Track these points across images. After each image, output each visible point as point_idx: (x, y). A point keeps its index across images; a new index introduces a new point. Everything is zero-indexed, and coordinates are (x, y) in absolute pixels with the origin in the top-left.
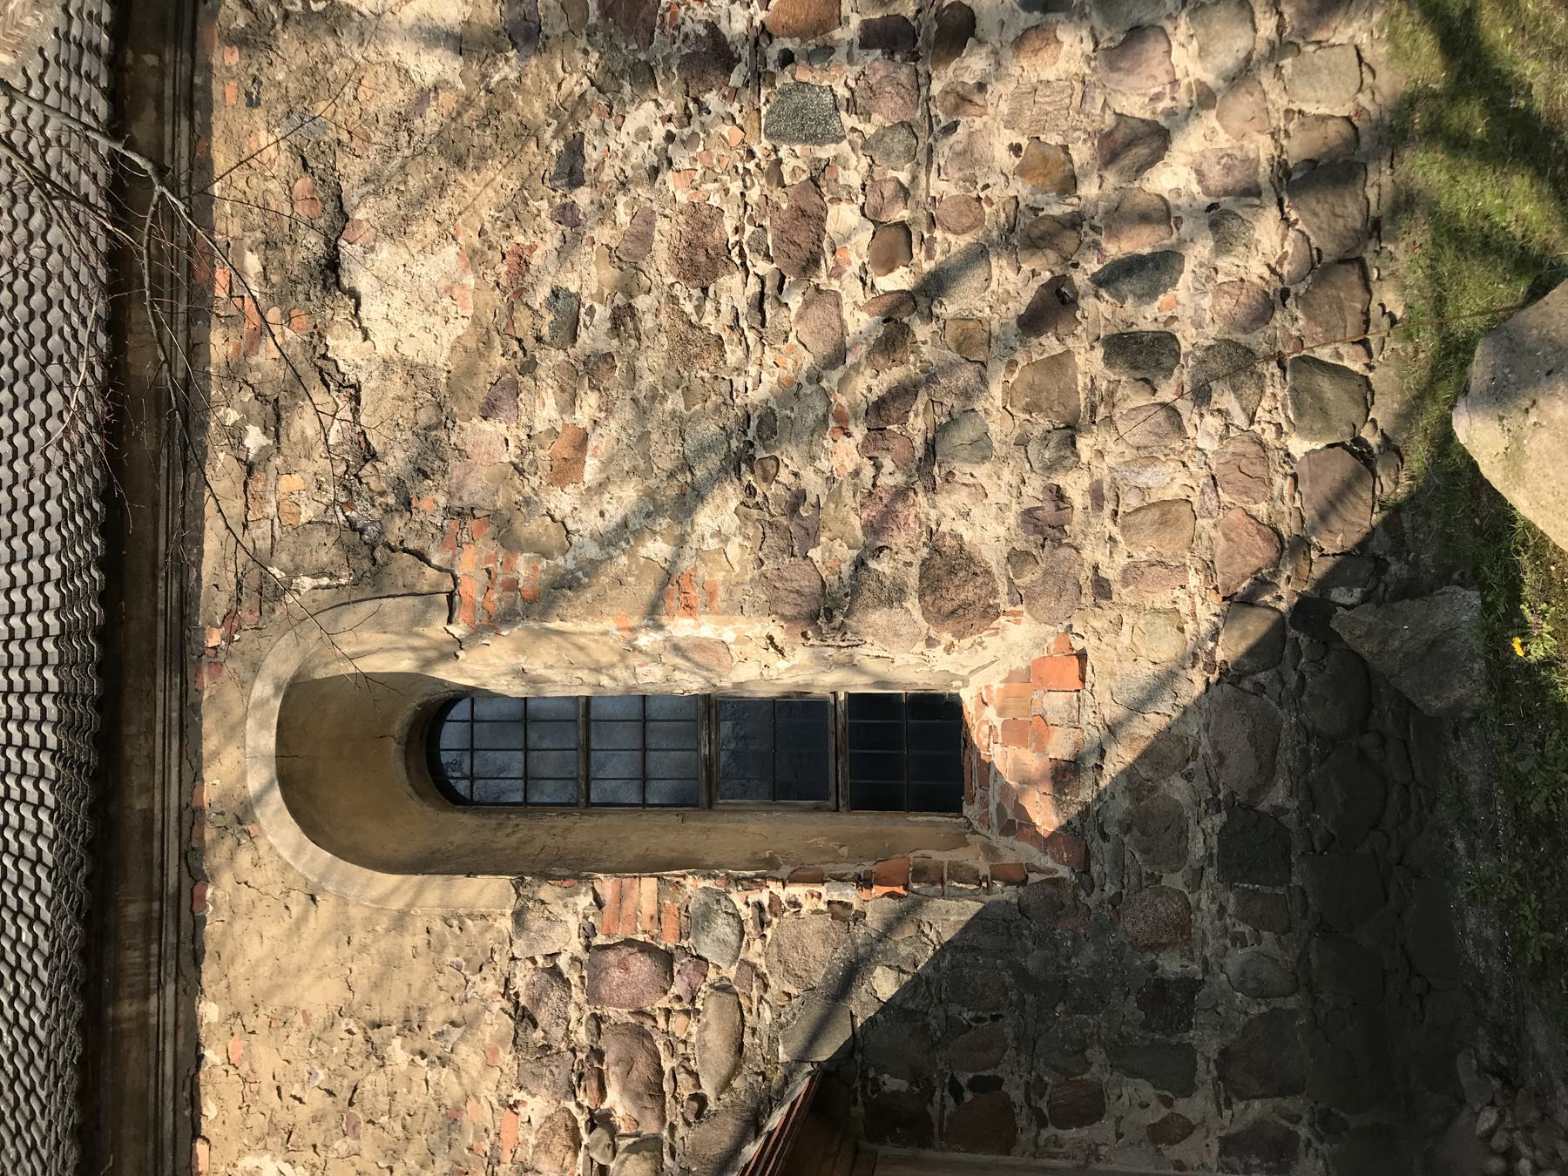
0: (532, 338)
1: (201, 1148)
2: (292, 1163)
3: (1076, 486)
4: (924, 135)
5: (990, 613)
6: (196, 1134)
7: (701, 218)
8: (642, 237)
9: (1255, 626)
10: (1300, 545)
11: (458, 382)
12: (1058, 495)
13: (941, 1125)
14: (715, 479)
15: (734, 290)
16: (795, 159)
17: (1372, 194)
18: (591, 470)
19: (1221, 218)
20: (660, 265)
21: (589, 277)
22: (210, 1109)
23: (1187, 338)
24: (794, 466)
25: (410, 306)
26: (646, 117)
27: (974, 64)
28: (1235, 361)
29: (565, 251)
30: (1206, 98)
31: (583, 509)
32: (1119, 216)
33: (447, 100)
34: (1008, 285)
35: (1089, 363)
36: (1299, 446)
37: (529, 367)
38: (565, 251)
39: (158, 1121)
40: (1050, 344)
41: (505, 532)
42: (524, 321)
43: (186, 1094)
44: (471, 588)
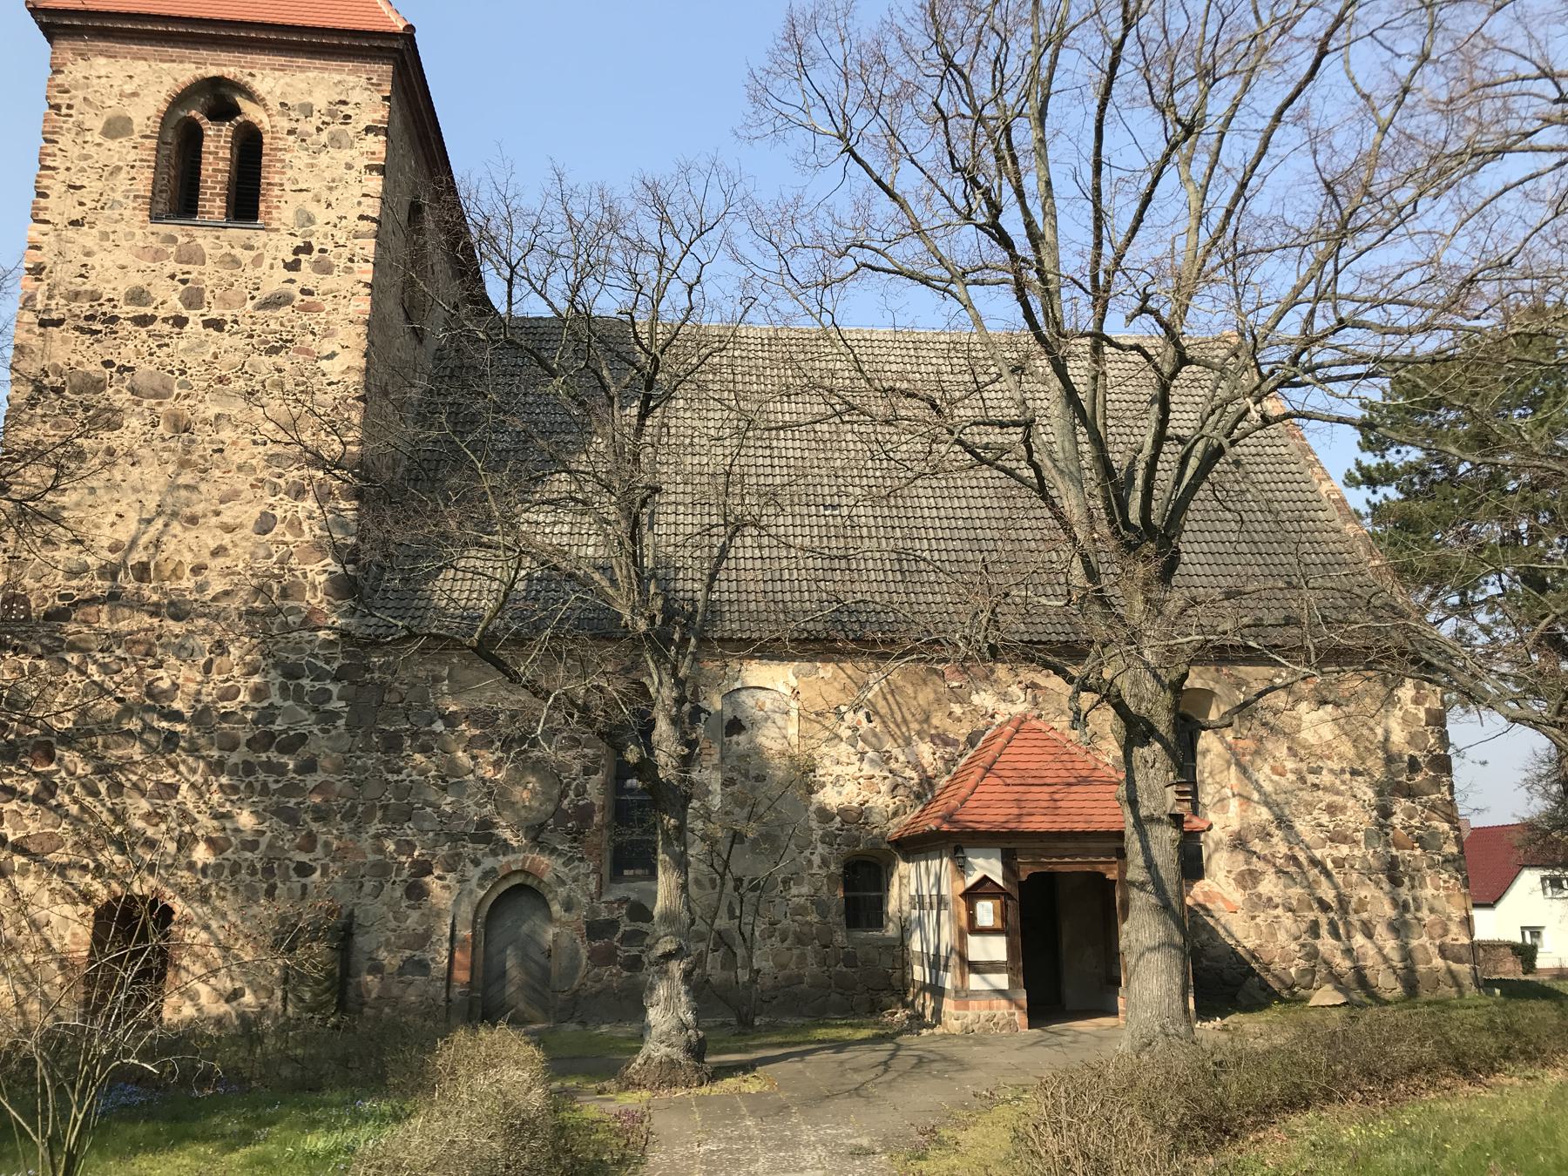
0: (1309, 760)
3: (1280, 911)
4: (1368, 872)
5: (1244, 888)
7: (1343, 809)
8: (1338, 793)
9: (1247, 957)
10: (1268, 970)
11: (1293, 740)
12: (1276, 907)
14: (1274, 814)
15: (1325, 819)
16: (1360, 836)
17: (1131, 59)
18: (1276, 778)
19: (1348, 952)
20: (1329, 798)
21: (1326, 778)
23: (1318, 943)
24: (1278, 836)
25: (1316, 725)
26: (1369, 795)
27: (1386, 886)
28: (1313, 954)
29: (1331, 771)
30: (1380, 950)
31: (1263, 773)
32: (1347, 924)
33: (1371, 737)
34: (1329, 895)
35: (1311, 916)
36: (1293, 970)
37: (1302, 760)
38: (1331, 771)
40: (1316, 906)
41: (1257, 753)
42: (1313, 759)
44: (1241, 743)
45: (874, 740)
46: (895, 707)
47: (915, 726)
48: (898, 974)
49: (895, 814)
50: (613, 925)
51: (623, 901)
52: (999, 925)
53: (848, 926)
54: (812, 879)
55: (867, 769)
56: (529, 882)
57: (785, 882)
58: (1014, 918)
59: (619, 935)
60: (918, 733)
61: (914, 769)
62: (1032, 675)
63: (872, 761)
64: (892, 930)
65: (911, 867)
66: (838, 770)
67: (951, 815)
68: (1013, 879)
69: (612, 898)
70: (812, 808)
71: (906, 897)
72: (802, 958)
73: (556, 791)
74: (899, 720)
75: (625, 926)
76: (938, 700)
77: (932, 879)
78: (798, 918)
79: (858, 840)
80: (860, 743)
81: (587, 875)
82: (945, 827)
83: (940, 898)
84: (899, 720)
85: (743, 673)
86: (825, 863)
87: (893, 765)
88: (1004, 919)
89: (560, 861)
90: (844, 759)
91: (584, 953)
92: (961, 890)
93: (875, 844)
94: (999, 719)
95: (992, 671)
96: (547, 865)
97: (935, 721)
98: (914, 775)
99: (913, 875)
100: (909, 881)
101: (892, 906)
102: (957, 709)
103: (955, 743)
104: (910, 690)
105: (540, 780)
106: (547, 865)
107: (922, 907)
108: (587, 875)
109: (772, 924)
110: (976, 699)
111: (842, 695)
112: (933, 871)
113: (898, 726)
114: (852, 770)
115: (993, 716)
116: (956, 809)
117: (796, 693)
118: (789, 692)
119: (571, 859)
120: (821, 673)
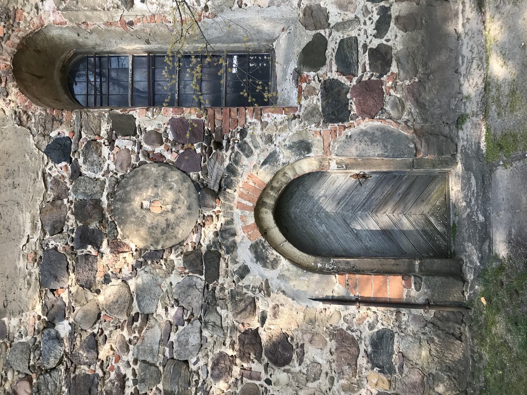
50: (330, 89)
59: (343, 79)
73: (154, 170)
75: (331, 71)
81: (264, 125)
96: (253, 175)
106: (253, 175)
108: (264, 125)
119: (243, 146)
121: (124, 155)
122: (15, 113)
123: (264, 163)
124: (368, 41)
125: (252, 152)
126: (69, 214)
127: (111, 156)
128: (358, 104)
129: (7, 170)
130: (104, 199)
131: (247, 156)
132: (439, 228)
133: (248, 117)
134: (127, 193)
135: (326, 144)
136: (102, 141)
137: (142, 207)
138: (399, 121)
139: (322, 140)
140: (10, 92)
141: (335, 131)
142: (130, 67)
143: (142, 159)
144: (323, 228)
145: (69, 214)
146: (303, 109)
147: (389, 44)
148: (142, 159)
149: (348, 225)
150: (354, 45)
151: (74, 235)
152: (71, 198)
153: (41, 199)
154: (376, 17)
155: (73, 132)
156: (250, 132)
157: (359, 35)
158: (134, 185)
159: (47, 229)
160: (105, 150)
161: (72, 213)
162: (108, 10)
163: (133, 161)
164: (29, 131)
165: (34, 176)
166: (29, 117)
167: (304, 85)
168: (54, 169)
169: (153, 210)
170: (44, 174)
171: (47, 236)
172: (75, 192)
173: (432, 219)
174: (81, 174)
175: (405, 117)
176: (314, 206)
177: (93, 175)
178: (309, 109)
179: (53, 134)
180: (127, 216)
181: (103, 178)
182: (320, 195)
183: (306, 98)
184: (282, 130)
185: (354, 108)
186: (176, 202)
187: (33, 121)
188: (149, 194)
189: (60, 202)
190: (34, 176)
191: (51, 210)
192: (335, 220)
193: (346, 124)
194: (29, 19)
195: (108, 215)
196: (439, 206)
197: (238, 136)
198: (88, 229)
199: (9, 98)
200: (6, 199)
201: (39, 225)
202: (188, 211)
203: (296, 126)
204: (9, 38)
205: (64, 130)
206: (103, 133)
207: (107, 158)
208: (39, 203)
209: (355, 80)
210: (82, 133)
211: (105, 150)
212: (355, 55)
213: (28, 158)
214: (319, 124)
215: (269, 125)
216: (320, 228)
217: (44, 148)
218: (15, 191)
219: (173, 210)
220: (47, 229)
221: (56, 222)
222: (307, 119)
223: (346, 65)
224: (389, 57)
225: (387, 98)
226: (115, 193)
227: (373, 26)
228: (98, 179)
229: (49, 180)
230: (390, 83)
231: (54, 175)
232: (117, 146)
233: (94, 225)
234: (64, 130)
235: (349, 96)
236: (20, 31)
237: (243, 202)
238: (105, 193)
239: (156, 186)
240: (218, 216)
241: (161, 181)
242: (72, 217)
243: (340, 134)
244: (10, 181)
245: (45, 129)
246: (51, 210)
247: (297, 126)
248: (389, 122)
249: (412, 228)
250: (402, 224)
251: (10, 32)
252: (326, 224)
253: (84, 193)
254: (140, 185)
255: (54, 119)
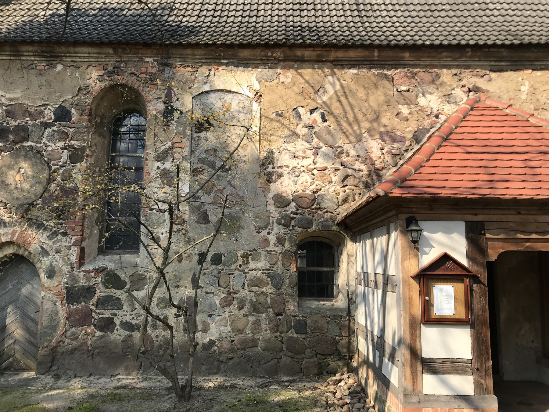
1: (530, 71)
2: (527, 94)
6: (533, 70)
13: (285, 211)
22: (539, 73)
39: (538, 61)
43: (543, 67)
45: (328, 137)
46: (348, 108)
47: (366, 125)
48: (344, 341)
49: (345, 201)
50: (89, 291)
51: (98, 271)
52: (462, 315)
53: (299, 296)
54: (263, 257)
55: (321, 162)
56: (21, 252)
57: (246, 257)
58: (480, 304)
59: (94, 300)
60: (369, 131)
61: (364, 162)
62: (475, 79)
63: (325, 155)
64: (340, 302)
65: (359, 245)
66: (294, 163)
67: (404, 180)
68: (479, 258)
69: (91, 268)
70: (270, 195)
71: (353, 273)
72: (257, 323)
73: (44, 176)
74: (351, 119)
75: (101, 292)
76: (388, 103)
77: (378, 257)
78: (255, 289)
79: (310, 223)
80: (315, 140)
81: (69, 248)
82: (396, 192)
83: (387, 279)
84: (351, 119)
85: (211, 78)
86: (280, 241)
87: (345, 159)
88: (469, 306)
89: (45, 235)
90: (300, 154)
91: (62, 313)
92: (414, 270)
93: (326, 228)
94: (443, 118)
95: (438, 76)
96: (36, 239)
97: (384, 120)
98: (363, 167)
99: (359, 254)
100: (356, 260)
101: (341, 280)
102: (405, 110)
103: (402, 140)
104: (361, 94)
105: (33, 165)
106: (36, 239)
107: (367, 285)
108: (69, 248)
109: (229, 293)
110: (422, 101)
111: (300, 98)
112: (379, 247)
113: (350, 124)
114: (307, 162)
115: (437, 117)
116: (409, 173)
117: (258, 95)
118: (251, 95)
119: (55, 234)
120: (282, 78)
121: (57, 156)
122: (88, 86)
123: (42, 248)
124: (119, 317)
125: (51, 240)
126: (19, 121)
127: (57, 148)
128: (77, 310)
129: (51, 81)
130: (30, 143)
131: (48, 237)
132: (4, 364)
133: (76, 237)
134: (30, 159)
135: (52, 289)
136: (67, 142)
137: (20, 168)
138: (63, 337)
139: (55, 286)
140: (102, 83)
141: (60, 295)
142: (137, 155)
143: (53, 168)
144: (10, 286)
145: (19, 121)
146: (77, 273)
147: (115, 331)
148: (53, 168)
149: (11, 303)
150: (116, 308)
151: (5, 124)
152: (29, 122)
153: (29, 104)
154: (134, 322)
155: (74, 123)
156: (64, 238)
157: (124, 311)
158: (36, 163)
159: (9, 108)
160: (61, 144)
161: (19, 123)
162: (155, 145)
163: (52, 162)
164: (75, 95)
165: (45, 98)
166: (85, 95)
167: (93, 274)
168: (49, 111)
169: (18, 175)
170: (47, 105)
171: (4, 108)
172: (33, 125)
173: (11, 359)
174: (45, 129)
175: (67, 341)
176: (26, 281)
177: (45, 136)
178: (77, 278)
179: (73, 111)
180: (15, 159)
181: (42, 142)
182: (34, 285)
183: (84, 275)
184: (64, 260)
185: (73, 307)
186: (22, 190)
187: (83, 97)
188: (29, 172)
189: (28, 115)
190: (45, 98)
191: (22, 110)
192: (15, 294)
193: (65, 302)
194: (151, 93)
195: (17, 146)
196: (19, 364)
197: (63, 231)
198: (9, 133)
199: (98, 82)
200: (32, 81)
201: (12, 103)
202: (15, 197)
203: (66, 269)
204: (138, 81)
205: (75, 117)
206: (73, 142)
207: (57, 145)
208: (27, 102)
209: (94, 308)
210: (73, 129)
211: (61, 144)
212: (109, 308)
213: (58, 94)
214: (67, 284)
215: (68, 251)
216: (10, 284)
217: (64, 104)
218: (37, 86)
219: (16, 188)
220: (9, 108)
221: (14, 113)
222: (70, 276)
223: (102, 303)
224: (106, 330)
225: (80, 328)
226: (32, 151)
227: (128, 320)
228: (42, 139)
229: (43, 108)
230: (89, 331)
231: (46, 111)
232: (63, 152)
233: (11, 137)
234: (75, 117)
235: (83, 303)
236: (143, 87)
237: (17, 234)
238: (32, 144)
239: (33, 177)
240: (10, 217)
241: (37, 180)
242: (16, 124)
243: (58, 298)
244: (44, 83)
245: (76, 105)
246: (22, 110)
247: (66, 270)
248: (63, 330)
249: (6, 345)
250: (9, 339)
251: (143, 81)
252: (13, 288)
253: (32, 131)
254: (35, 167)
255: (83, 111)
